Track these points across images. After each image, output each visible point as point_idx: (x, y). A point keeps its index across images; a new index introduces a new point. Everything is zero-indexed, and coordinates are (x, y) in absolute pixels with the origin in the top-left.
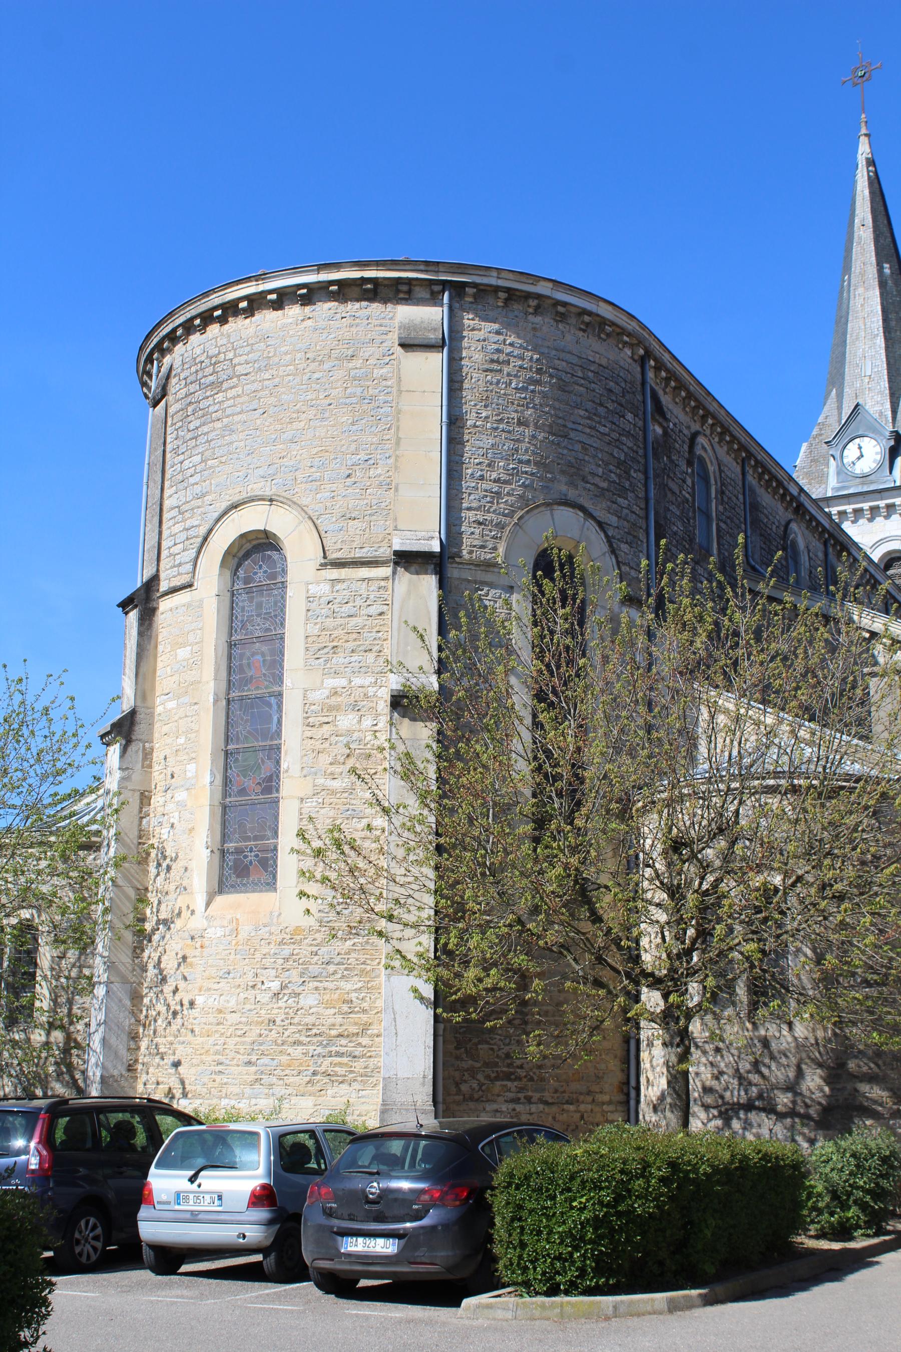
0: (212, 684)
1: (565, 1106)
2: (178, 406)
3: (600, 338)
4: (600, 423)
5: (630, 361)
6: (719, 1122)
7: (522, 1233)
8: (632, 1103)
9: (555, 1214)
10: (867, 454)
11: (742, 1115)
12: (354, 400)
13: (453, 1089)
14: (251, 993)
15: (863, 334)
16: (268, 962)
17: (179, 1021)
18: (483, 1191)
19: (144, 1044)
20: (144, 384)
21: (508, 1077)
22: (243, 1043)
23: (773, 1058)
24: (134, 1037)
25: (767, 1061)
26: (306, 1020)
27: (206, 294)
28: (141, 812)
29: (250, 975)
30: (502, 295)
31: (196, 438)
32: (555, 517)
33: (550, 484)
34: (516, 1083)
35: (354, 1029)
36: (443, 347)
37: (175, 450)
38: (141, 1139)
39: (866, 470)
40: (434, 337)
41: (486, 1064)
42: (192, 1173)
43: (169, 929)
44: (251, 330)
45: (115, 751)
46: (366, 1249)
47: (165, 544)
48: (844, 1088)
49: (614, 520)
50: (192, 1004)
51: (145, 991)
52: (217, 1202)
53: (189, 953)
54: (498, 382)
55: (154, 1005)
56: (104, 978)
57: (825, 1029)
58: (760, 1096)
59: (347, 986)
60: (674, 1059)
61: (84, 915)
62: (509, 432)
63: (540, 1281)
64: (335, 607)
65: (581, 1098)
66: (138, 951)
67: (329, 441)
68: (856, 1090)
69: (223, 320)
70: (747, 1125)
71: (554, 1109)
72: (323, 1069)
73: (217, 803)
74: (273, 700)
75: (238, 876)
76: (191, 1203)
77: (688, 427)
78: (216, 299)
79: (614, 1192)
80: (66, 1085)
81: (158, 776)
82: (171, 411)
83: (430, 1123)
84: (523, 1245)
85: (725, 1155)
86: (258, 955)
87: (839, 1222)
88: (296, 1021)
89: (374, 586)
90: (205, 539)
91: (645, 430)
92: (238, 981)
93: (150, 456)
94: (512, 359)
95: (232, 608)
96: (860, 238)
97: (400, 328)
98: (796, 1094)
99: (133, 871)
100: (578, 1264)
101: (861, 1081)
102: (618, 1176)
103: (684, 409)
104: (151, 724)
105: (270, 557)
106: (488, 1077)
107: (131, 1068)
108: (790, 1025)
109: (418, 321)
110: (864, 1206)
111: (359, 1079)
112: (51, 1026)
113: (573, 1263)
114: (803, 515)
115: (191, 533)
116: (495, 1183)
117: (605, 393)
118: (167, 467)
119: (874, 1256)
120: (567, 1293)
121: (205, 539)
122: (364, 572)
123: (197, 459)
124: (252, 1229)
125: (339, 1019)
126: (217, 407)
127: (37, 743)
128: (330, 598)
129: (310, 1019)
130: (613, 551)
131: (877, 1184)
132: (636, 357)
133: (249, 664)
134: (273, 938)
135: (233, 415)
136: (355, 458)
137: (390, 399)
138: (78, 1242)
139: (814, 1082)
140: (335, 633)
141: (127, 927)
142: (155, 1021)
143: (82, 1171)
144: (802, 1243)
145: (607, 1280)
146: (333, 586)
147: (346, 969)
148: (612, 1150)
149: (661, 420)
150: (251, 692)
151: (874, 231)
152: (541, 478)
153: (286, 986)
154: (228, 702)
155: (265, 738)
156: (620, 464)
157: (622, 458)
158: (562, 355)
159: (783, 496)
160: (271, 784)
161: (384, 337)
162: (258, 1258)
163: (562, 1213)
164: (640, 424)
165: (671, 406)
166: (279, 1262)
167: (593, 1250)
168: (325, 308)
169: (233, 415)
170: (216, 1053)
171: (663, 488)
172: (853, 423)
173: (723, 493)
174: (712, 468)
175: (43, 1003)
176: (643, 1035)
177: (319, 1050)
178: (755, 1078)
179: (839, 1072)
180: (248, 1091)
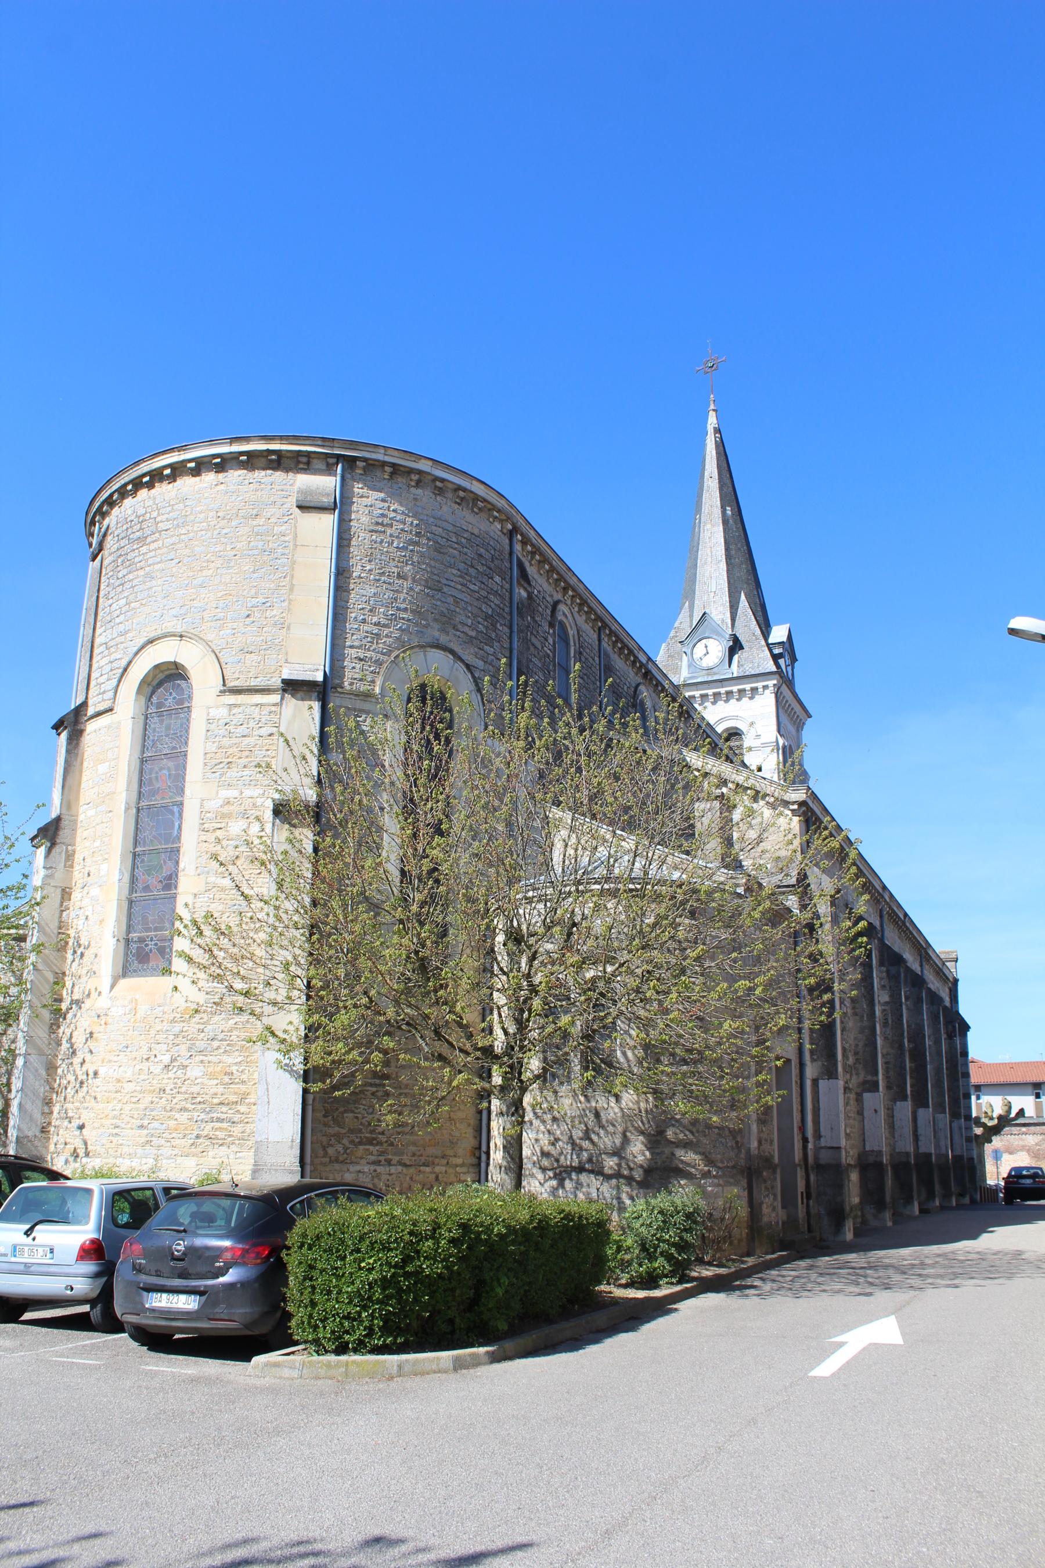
0: (124, 794)
1: (422, 1168)
2: (111, 558)
3: (473, 511)
4: (470, 582)
5: (499, 533)
6: (554, 1183)
7: (313, 1292)
8: (483, 1165)
9: (344, 1273)
10: (711, 652)
11: (574, 1176)
12: (255, 552)
13: (321, 1152)
14: (146, 1064)
15: (709, 559)
16: (161, 1038)
17: (85, 1089)
19: (56, 1109)
21: (370, 1142)
22: (137, 1109)
23: (602, 1127)
24: (48, 1103)
25: (596, 1129)
26: (192, 1090)
27: (137, 463)
28: (61, 906)
29: (145, 1048)
30: (388, 469)
31: (122, 584)
32: (428, 657)
33: (424, 630)
34: (377, 1148)
35: (233, 1098)
36: (334, 510)
39: (711, 665)
40: (328, 500)
42: (28, 1227)
43: (80, 1008)
44: (173, 493)
46: (169, 1305)
47: (94, 676)
48: (662, 1153)
49: (480, 664)
50: (96, 1073)
51: (60, 1062)
52: (49, 1255)
53: (95, 1029)
54: (382, 542)
55: (65, 1075)
56: (23, 1051)
57: (647, 1101)
58: (590, 1160)
59: (229, 1060)
62: (389, 584)
63: (329, 1339)
64: (231, 728)
65: (437, 1161)
66: (54, 1027)
67: (234, 588)
68: (673, 1154)
69: (150, 485)
70: (579, 1185)
71: (412, 1170)
72: (205, 1133)
73: (124, 898)
74: (176, 809)
75: (140, 962)
76: (26, 1255)
77: (551, 596)
79: (402, 1253)
81: (78, 875)
82: (105, 563)
85: (524, 1215)
86: (153, 1032)
87: (647, 1272)
88: (183, 1090)
89: (266, 710)
90: (125, 670)
91: (511, 592)
93: (88, 602)
94: (395, 523)
95: (145, 729)
96: (708, 487)
97: (298, 492)
98: (621, 1158)
99: (52, 958)
100: (366, 1323)
101: (677, 1147)
102: (407, 1237)
103: (539, 571)
104: (74, 830)
105: (179, 685)
106: (352, 1142)
107: (44, 1130)
108: (617, 1097)
109: (314, 488)
110: (669, 1258)
111: (237, 1142)
114: (651, 679)
115: (115, 665)
117: (476, 557)
118: (100, 610)
119: (675, 1303)
120: (355, 1351)
121: (125, 670)
122: (258, 698)
123: (123, 602)
126: (141, 558)
128: (228, 720)
129: (195, 1089)
131: (681, 1238)
132: (505, 531)
133: (157, 778)
134: (166, 1016)
135: (154, 564)
136: (254, 601)
137: (287, 552)
139: (638, 1151)
140: (230, 751)
141: (45, 1006)
142: (66, 1088)
144: (610, 1292)
145: (395, 1339)
146: (230, 710)
147: (228, 1045)
149: (526, 585)
150: (157, 801)
151: (720, 482)
152: (416, 624)
153: (176, 1059)
154: (138, 810)
155: (167, 842)
156: (487, 617)
157: (490, 613)
158: (439, 523)
159: (634, 662)
160: (170, 882)
161: (285, 500)
162: (86, 1308)
163: (351, 1273)
164: (507, 586)
165: (536, 577)
167: (380, 1310)
168: (235, 476)
169: (154, 564)
170: (114, 1118)
171: (526, 642)
173: (580, 653)
174: (572, 632)
177: (203, 1116)
178: (586, 1144)
179: (659, 1138)
180: (140, 1151)
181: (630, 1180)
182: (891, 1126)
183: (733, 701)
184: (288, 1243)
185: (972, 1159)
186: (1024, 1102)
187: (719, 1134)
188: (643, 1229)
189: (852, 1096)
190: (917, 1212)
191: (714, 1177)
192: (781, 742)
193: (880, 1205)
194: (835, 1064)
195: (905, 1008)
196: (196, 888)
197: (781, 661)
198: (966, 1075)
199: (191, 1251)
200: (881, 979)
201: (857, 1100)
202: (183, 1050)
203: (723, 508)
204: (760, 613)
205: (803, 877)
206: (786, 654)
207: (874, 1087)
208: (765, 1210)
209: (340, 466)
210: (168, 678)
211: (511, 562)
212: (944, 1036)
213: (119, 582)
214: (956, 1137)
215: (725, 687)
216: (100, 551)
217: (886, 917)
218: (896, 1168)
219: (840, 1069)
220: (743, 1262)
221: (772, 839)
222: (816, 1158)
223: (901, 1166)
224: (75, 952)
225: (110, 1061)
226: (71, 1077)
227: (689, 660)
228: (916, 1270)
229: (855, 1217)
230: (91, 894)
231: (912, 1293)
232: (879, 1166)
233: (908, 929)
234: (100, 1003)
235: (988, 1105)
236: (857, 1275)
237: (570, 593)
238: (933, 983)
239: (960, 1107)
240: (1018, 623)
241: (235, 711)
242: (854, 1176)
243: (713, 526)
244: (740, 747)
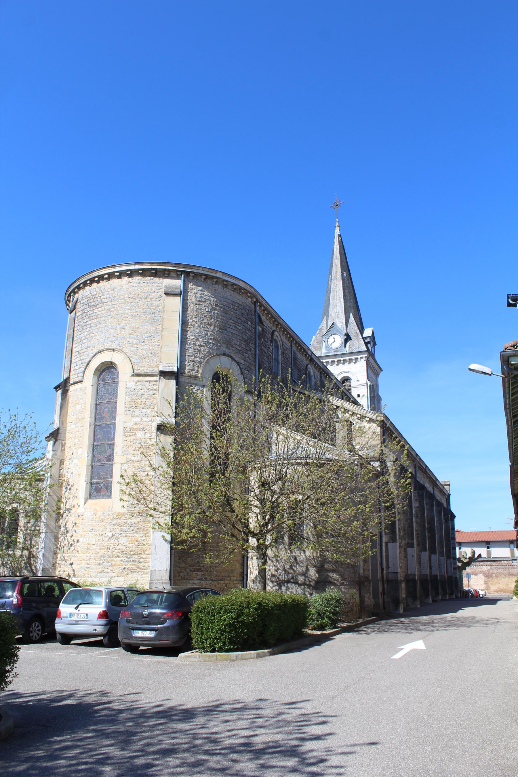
6: (277, 587)
8: (245, 580)
10: (336, 341)
12: (146, 313)
13: (177, 575)
14: (101, 537)
16: (107, 526)
17: (73, 547)
18: (187, 613)
19: (59, 556)
20: (67, 305)
21: (198, 570)
22: (97, 556)
23: (297, 564)
24: (55, 554)
25: (295, 565)
26: (121, 548)
30: (204, 277)
31: (86, 325)
35: (140, 552)
37: (78, 330)
38: (57, 592)
39: (336, 347)
40: (177, 291)
41: (190, 566)
42: (76, 606)
43: (70, 512)
44: (109, 286)
45: (51, 443)
47: (72, 366)
49: (242, 362)
50: (78, 541)
51: (60, 536)
52: (86, 617)
54: (201, 309)
55: (63, 541)
56: (44, 530)
57: (317, 553)
58: (292, 578)
60: (261, 564)
61: (37, 506)
62: (204, 328)
65: (226, 578)
67: (136, 329)
68: (328, 575)
69: (98, 282)
71: (216, 582)
72: (128, 566)
74: (112, 426)
77: (271, 328)
78: (96, 274)
79: (237, 614)
80: (29, 571)
81: (67, 453)
82: (77, 315)
83: (168, 587)
84: (202, 634)
85: (279, 600)
86: (104, 523)
88: (118, 548)
89: (152, 384)
90: (88, 364)
91: (255, 328)
92: (96, 533)
95: (97, 390)
96: (335, 262)
98: (306, 577)
100: (223, 640)
102: (238, 608)
104: (65, 434)
105: (112, 371)
106: (190, 570)
107: (54, 565)
108: (304, 551)
109: (171, 285)
110: (329, 618)
112: (23, 549)
113: (221, 640)
115: (83, 361)
116: (192, 610)
118: (75, 336)
120: (218, 651)
121: (88, 364)
123: (86, 333)
124: (99, 627)
125: (134, 548)
126: (94, 314)
127: (21, 440)
129: (123, 548)
130: (242, 373)
133: (103, 412)
134: (110, 516)
135: (100, 317)
138: (32, 632)
139: (313, 573)
140: (137, 401)
142: (64, 547)
143: (34, 605)
146: (136, 383)
148: (236, 598)
150: (104, 423)
152: (216, 345)
153: (114, 535)
154: (95, 426)
155: (108, 440)
156: (246, 341)
159: (306, 355)
160: (110, 458)
162: (101, 638)
164: (254, 326)
166: (109, 640)
168: (137, 279)
169: (100, 317)
170: (87, 560)
171: (261, 350)
172: (332, 329)
173: (283, 353)
174: (279, 344)
175: (21, 540)
176: (249, 555)
177: (126, 559)
178: (291, 571)
180: (99, 574)
181: (309, 586)
182: (419, 563)
183: (346, 364)
184: (192, 610)
185: (456, 578)
186: (481, 551)
187: (347, 567)
188: (319, 606)
189: (402, 549)
190: (431, 602)
191: (345, 585)
192: (369, 383)
193: (415, 598)
194: (396, 536)
195: (426, 507)
196: (124, 460)
197: (369, 345)
198: (454, 539)
199: (150, 614)
200: (415, 496)
201: (404, 551)
202: (117, 531)
203: (342, 273)
204: (359, 323)
205: (382, 454)
206: (371, 342)
207: (412, 545)
208: (366, 599)
209: (183, 276)
210: (107, 369)
211: (255, 315)
212: (443, 521)
213: (84, 324)
214: (449, 568)
215: (341, 358)
216: (74, 310)
217: (417, 468)
218: (421, 581)
219: (398, 538)
220: (358, 621)
221: (368, 437)
222: (387, 577)
223: (424, 581)
224: (67, 488)
225: (85, 536)
226: (66, 542)
227: (324, 345)
228: (431, 624)
229: (404, 603)
230: (74, 462)
231: (429, 632)
232: (414, 580)
233: (427, 472)
234: (80, 510)
235: (464, 552)
236: (405, 626)
237: (279, 326)
238: (439, 496)
239: (450, 554)
240: (473, 366)
241: (138, 383)
242: (403, 585)
243: (337, 281)
244: (350, 386)
